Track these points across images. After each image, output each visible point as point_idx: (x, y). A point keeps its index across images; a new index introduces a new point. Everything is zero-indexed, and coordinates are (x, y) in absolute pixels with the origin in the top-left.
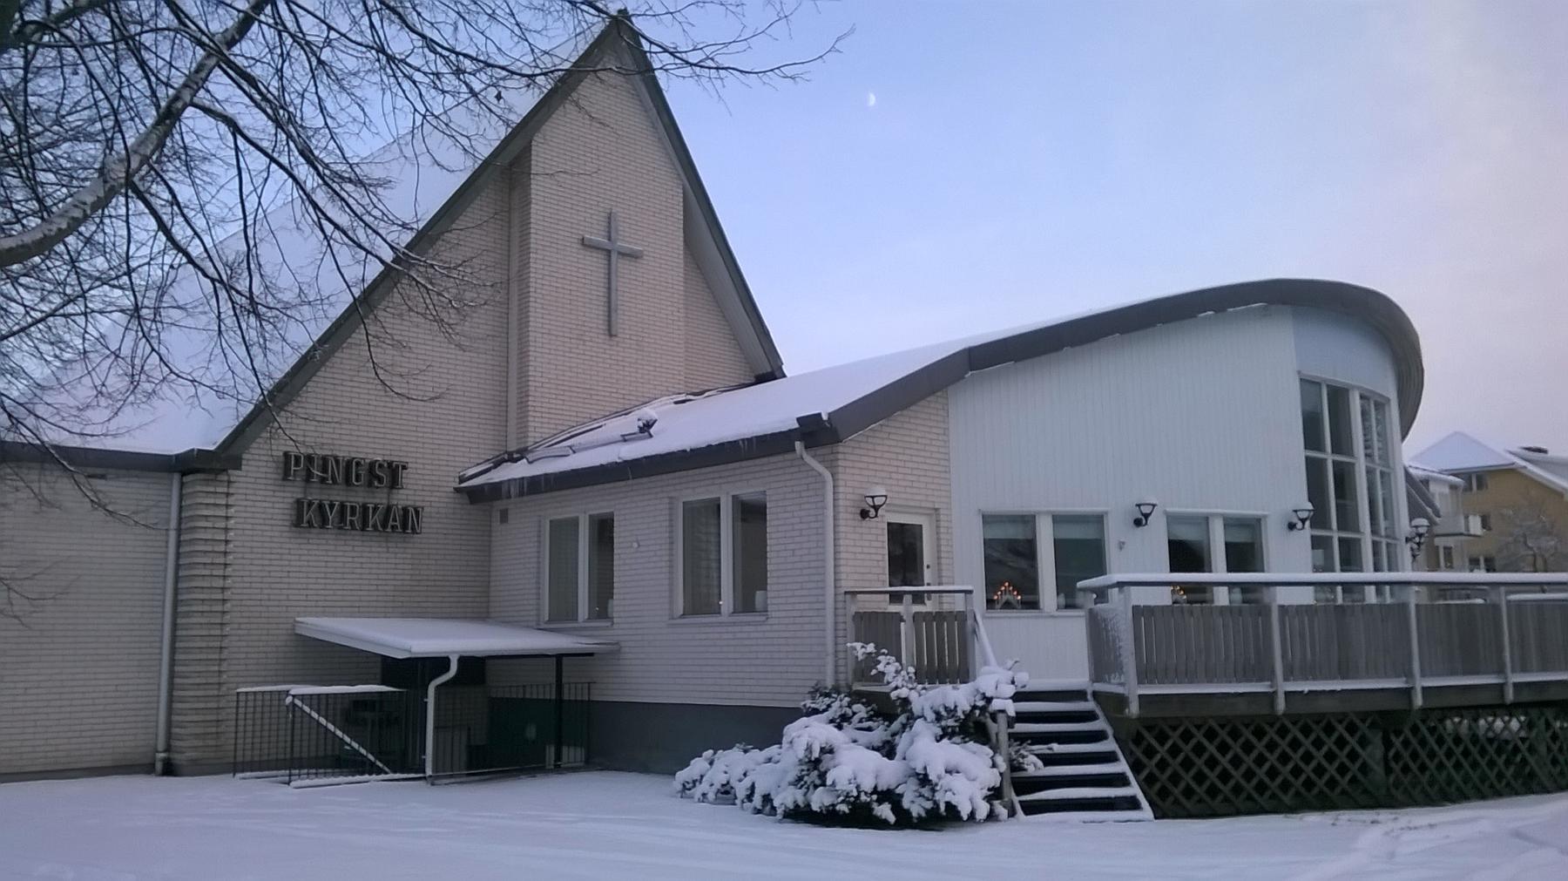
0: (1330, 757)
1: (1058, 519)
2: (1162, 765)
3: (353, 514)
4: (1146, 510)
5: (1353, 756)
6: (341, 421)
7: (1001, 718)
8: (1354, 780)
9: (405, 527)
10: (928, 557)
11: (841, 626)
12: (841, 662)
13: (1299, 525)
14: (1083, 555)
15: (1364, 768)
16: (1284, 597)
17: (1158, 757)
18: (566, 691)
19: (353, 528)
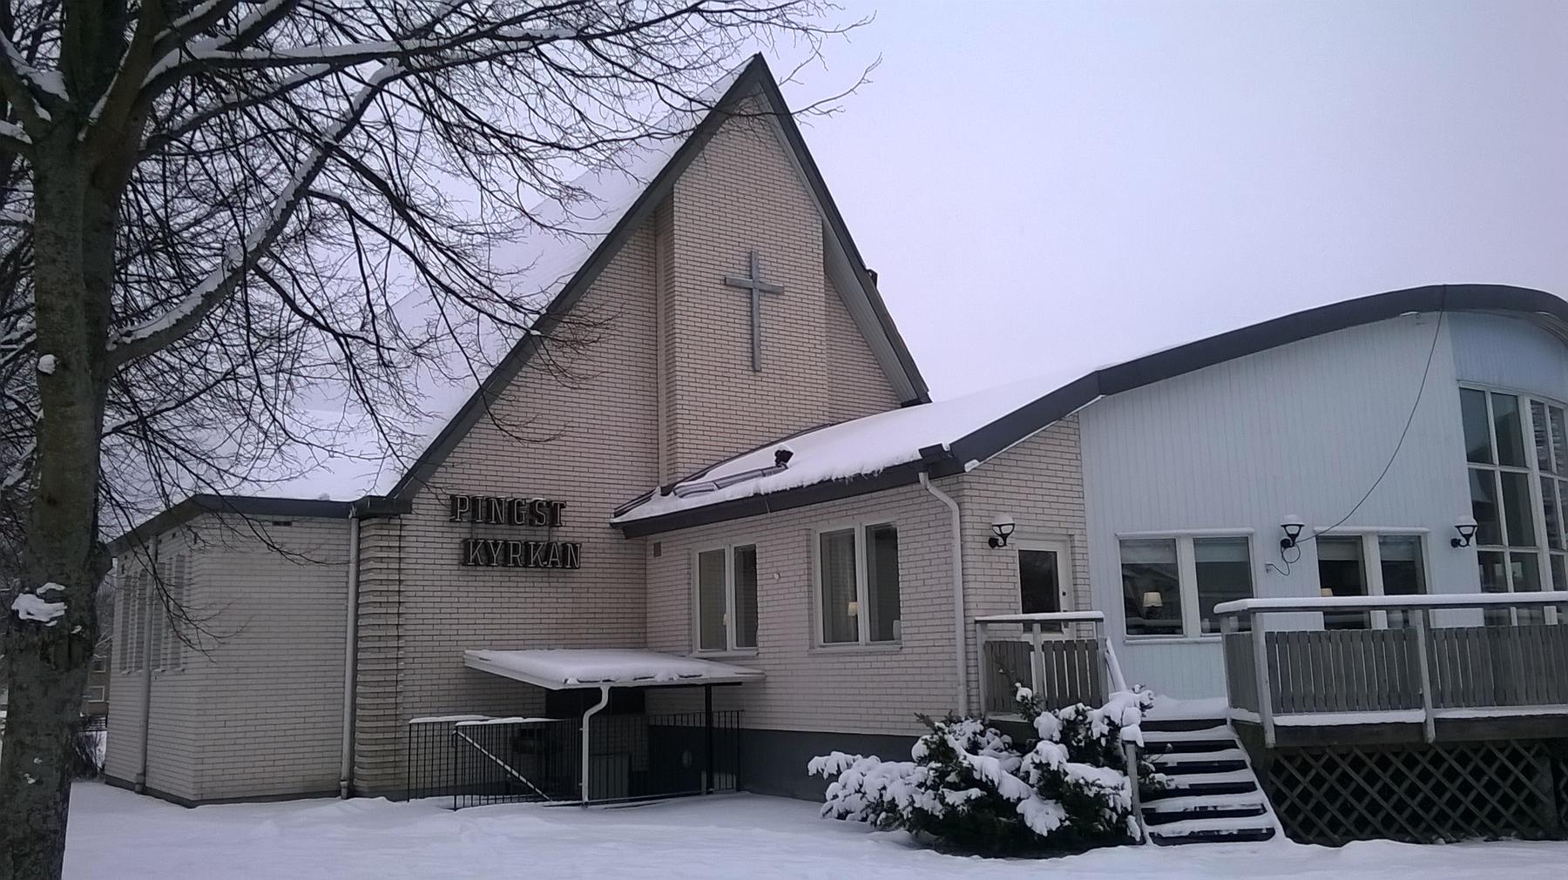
0: (1492, 787)
1: (1199, 542)
2: (1305, 796)
3: (515, 552)
4: (1293, 530)
5: (1518, 786)
6: (492, 470)
7: (1130, 749)
8: (1520, 811)
9: (564, 562)
10: (1063, 584)
11: (972, 656)
12: (974, 692)
13: (1463, 542)
14: (1227, 575)
15: (1532, 800)
16: (1442, 620)
17: (1300, 788)
18: (715, 719)
19: (517, 565)
